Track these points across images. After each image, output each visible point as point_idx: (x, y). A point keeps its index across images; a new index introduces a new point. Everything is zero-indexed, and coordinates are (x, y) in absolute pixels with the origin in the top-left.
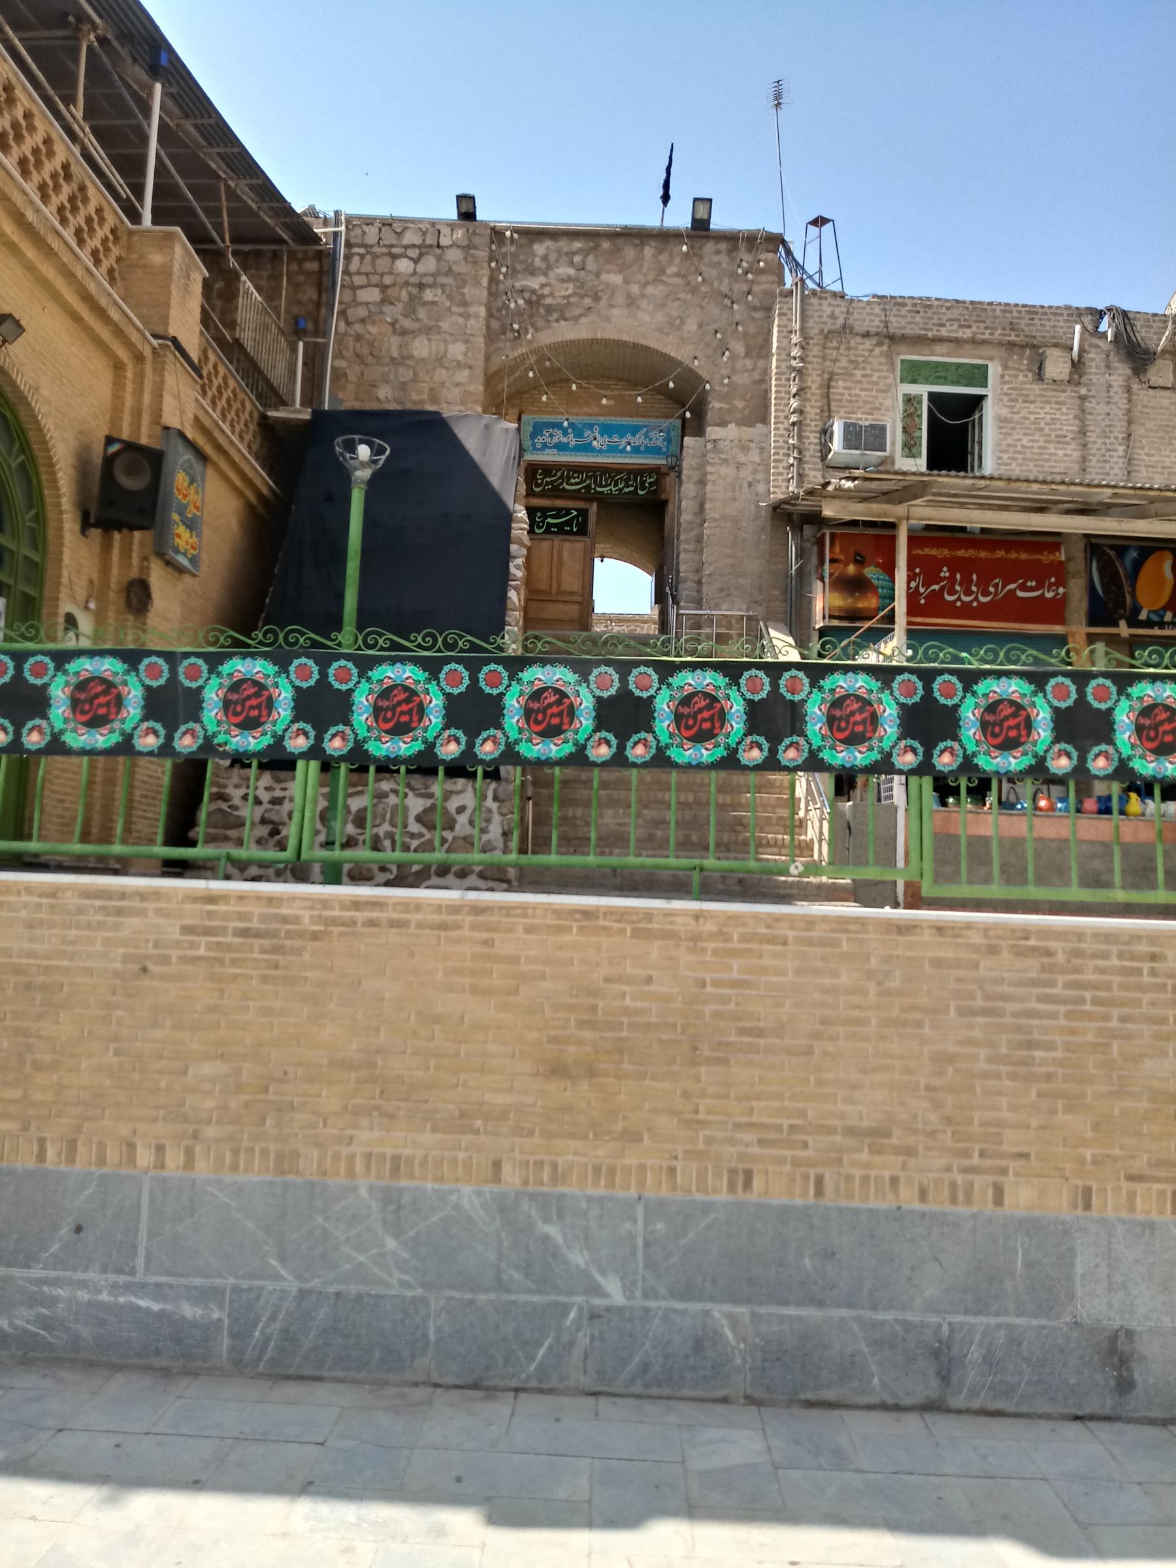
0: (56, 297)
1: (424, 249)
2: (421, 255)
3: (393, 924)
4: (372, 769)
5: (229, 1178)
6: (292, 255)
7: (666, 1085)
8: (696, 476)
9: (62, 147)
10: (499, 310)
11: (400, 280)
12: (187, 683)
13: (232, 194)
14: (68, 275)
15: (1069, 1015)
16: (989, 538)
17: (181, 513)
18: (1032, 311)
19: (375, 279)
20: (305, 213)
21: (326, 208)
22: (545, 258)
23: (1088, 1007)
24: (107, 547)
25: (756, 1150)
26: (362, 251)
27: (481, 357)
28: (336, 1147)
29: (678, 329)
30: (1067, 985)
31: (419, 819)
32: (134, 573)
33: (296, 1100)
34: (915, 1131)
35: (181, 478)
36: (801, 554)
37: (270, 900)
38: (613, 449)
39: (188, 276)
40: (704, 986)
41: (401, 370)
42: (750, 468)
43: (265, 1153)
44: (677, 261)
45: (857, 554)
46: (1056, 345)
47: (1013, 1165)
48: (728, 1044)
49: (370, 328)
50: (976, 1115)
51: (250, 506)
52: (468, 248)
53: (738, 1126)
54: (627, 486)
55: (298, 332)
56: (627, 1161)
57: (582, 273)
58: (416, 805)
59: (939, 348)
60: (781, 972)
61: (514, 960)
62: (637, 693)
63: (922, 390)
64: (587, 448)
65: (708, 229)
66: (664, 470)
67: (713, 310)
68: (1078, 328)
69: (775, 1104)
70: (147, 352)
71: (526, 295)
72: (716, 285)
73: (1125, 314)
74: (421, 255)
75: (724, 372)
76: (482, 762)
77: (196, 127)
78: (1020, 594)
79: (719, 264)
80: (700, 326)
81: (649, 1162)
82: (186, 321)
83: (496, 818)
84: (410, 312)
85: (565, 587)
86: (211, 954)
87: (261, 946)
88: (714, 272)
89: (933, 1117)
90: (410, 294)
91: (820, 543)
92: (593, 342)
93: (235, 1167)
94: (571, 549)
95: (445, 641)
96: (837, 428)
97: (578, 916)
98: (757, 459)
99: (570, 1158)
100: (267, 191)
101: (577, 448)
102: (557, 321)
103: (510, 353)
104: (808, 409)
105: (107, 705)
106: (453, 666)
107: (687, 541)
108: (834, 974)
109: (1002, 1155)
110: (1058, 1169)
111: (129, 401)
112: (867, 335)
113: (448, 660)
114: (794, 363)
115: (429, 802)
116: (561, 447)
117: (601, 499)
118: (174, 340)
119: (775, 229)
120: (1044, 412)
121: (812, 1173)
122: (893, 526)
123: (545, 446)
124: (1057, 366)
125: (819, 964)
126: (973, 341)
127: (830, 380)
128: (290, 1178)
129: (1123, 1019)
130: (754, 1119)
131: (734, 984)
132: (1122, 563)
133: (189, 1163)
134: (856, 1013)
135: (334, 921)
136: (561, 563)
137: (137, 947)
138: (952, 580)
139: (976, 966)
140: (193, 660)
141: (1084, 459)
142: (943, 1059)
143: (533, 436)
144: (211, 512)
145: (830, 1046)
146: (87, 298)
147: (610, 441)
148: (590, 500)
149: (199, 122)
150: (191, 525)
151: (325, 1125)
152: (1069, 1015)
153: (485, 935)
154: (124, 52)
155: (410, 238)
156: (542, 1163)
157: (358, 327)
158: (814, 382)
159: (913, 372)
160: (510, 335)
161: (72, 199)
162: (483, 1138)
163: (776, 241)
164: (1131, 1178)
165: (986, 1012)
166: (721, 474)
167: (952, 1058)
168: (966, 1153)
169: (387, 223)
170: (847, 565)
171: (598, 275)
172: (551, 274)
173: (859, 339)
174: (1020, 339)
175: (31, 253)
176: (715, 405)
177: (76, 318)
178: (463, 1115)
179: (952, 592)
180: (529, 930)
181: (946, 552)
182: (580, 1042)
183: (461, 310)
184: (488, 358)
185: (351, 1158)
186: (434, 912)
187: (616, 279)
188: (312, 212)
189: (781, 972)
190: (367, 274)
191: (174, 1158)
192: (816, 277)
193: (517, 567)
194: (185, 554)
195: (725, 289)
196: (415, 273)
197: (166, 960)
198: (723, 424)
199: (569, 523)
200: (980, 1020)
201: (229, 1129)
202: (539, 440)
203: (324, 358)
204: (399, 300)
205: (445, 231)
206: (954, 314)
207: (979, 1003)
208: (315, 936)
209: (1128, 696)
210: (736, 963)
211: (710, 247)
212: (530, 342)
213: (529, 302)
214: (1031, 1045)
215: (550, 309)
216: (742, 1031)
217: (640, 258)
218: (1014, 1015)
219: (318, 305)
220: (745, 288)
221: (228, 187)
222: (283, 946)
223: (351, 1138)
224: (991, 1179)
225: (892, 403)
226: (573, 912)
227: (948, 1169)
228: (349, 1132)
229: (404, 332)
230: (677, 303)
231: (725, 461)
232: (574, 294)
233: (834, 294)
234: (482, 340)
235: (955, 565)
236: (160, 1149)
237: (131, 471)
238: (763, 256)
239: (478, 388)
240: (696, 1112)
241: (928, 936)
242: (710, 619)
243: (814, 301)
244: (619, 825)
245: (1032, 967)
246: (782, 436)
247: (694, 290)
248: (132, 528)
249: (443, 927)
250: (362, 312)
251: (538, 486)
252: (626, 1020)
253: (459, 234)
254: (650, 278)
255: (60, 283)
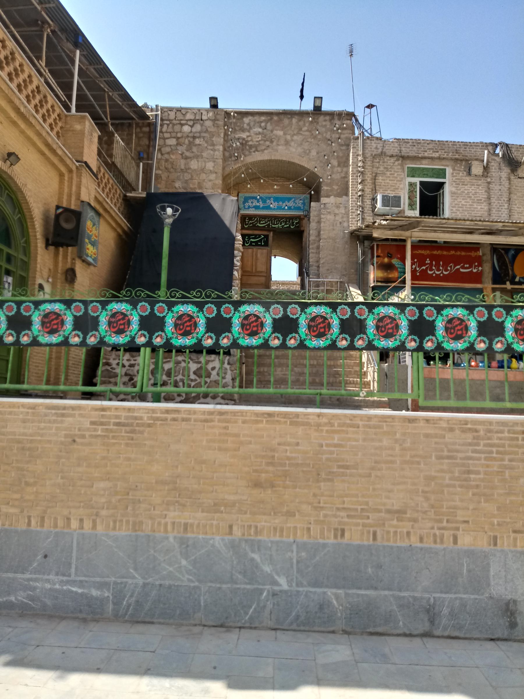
0: (34, 144)
1: (195, 121)
2: (194, 124)
3: (183, 420)
4: (174, 351)
5: (112, 533)
6: (137, 125)
7: (306, 491)
8: (316, 219)
9: (36, 79)
10: (229, 147)
11: (185, 135)
12: (92, 314)
13: (110, 98)
14: (39, 135)
15: (486, 459)
16: (448, 246)
17: (89, 239)
18: (465, 144)
19: (174, 135)
20: (143, 106)
21: (152, 104)
22: (249, 124)
23: (494, 455)
24: (56, 255)
25: (346, 520)
26: (168, 122)
27: (221, 168)
28: (159, 520)
29: (308, 154)
30: (485, 445)
31: (195, 373)
32: (69, 266)
33: (141, 499)
34: (418, 511)
35: (89, 224)
36: (363, 253)
37: (129, 409)
38: (280, 208)
39: (92, 135)
40: (322, 447)
41: (186, 174)
42: (341, 216)
43: (128, 522)
44: (307, 125)
45: (388, 253)
46: (476, 160)
47: (462, 526)
48: (333, 472)
49: (172, 156)
50: (445, 503)
51: (119, 235)
52: (214, 120)
53: (338, 509)
54: (286, 224)
55: (140, 159)
56: (289, 525)
57: (265, 131)
58: (193, 367)
59: (424, 162)
60: (357, 440)
61: (237, 435)
62: (291, 316)
63: (417, 180)
64: (268, 208)
65: (321, 110)
66: (302, 217)
67: (323, 146)
68: (486, 152)
69: (354, 499)
70: (74, 168)
71: (241, 141)
72: (324, 135)
73: (507, 145)
74: (194, 124)
75: (329, 173)
76: (223, 347)
77: (94, 69)
78: (462, 270)
79: (325, 126)
80: (318, 153)
81: (298, 526)
82: (91, 155)
83: (229, 372)
84: (189, 149)
85: (259, 269)
86: (103, 434)
87: (125, 430)
88: (324, 129)
89: (425, 505)
90: (189, 141)
91: (372, 248)
92: (270, 161)
93: (114, 529)
94: (261, 252)
95: (206, 294)
96: (379, 198)
97: (266, 416)
98: (343, 211)
99: (263, 523)
100: (126, 97)
101: (264, 208)
102: (254, 152)
103: (233, 166)
104: (366, 189)
105: (57, 324)
106: (209, 305)
107: (313, 248)
108: (380, 441)
109: (457, 522)
110: (482, 528)
111: (66, 190)
112: (392, 156)
113: (207, 303)
114: (359, 169)
115: (199, 365)
116: (257, 208)
117: (274, 230)
118: (86, 163)
119: (350, 110)
120: (472, 189)
121: (372, 530)
122: (404, 241)
123: (249, 207)
124: (477, 169)
125: (374, 436)
126: (439, 158)
127: (375, 176)
128: (139, 533)
129: (511, 460)
130: (345, 506)
131: (336, 446)
132: (508, 256)
133: (94, 527)
134: (390, 458)
135: (157, 419)
136: (257, 259)
137: (71, 431)
138: (431, 264)
139: (444, 437)
140: (95, 304)
141: (490, 210)
142: (429, 479)
143: (244, 203)
144: (101, 239)
145: (379, 473)
146: (48, 145)
147: (279, 205)
148: (270, 231)
149: (96, 67)
150: (93, 244)
151: (154, 510)
152: (486, 459)
153: (224, 425)
154: (63, 37)
155: (189, 116)
156: (251, 526)
157: (166, 156)
158: (368, 177)
159: (413, 173)
160: (233, 158)
161: (41, 102)
162: (224, 515)
163: (351, 115)
164: (515, 532)
165: (449, 457)
166: (327, 219)
167: (433, 478)
168: (440, 521)
169: (179, 110)
170: (384, 258)
171: (272, 131)
172: (252, 131)
173: (388, 158)
174: (460, 157)
175: (23, 126)
176: (324, 188)
177: (43, 154)
178: (215, 505)
179: (431, 270)
180: (244, 422)
181: (428, 252)
182: (267, 472)
183: (212, 148)
184: (224, 168)
185: (166, 524)
186: (202, 414)
187: (280, 133)
188: (146, 105)
189: (357, 440)
190: (170, 133)
191: (88, 525)
192: (369, 131)
193: (238, 261)
194: (91, 257)
195: (328, 136)
196: (191, 132)
197: (83, 437)
198: (328, 196)
199: (260, 241)
200: (446, 461)
201: (111, 511)
202: (247, 205)
203: (151, 169)
204: (184, 143)
205: (204, 113)
206: (431, 146)
207: (446, 453)
208: (149, 426)
209: (511, 316)
210: (336, 436)
211: (321, 118)
212: (242, 161)
213: (242, 144)
214: (469, 472)
215: (251, 147)
216: (339, 467)
217: (290, 124)
218: (461, 459)
219: (149, 146)
220: (337, 136)
221: (109, 95)
222: (135, 430)
223: (166, 515)
224: (452, 532)
225: (403, 187)
226: (263, 414)
227: (433, 528)
228: (165, 512)
229: (186, 158)
230: (307, 143)
231: (329, 213)
232: (262, 140)
233: (377, 138)
234: (221, 161)
235: (432, 258)
236: (81, 520)
237: (67, 221)
238: (345, 122)
239: (219, 182)
240: (319, 503)
241: (422, 424)
242: (323, 283)
243: (368, 141)
244: (284, 375)
245: (469, 437)
246: (354, 201)
247: (315, 137)
248: (68, 245)
249: (206, 421)
250: (168, 149)
251: (246, 225)
252: (287, 462)
253: (211, 114)
254: (295, 132)
255: (35, 138)
